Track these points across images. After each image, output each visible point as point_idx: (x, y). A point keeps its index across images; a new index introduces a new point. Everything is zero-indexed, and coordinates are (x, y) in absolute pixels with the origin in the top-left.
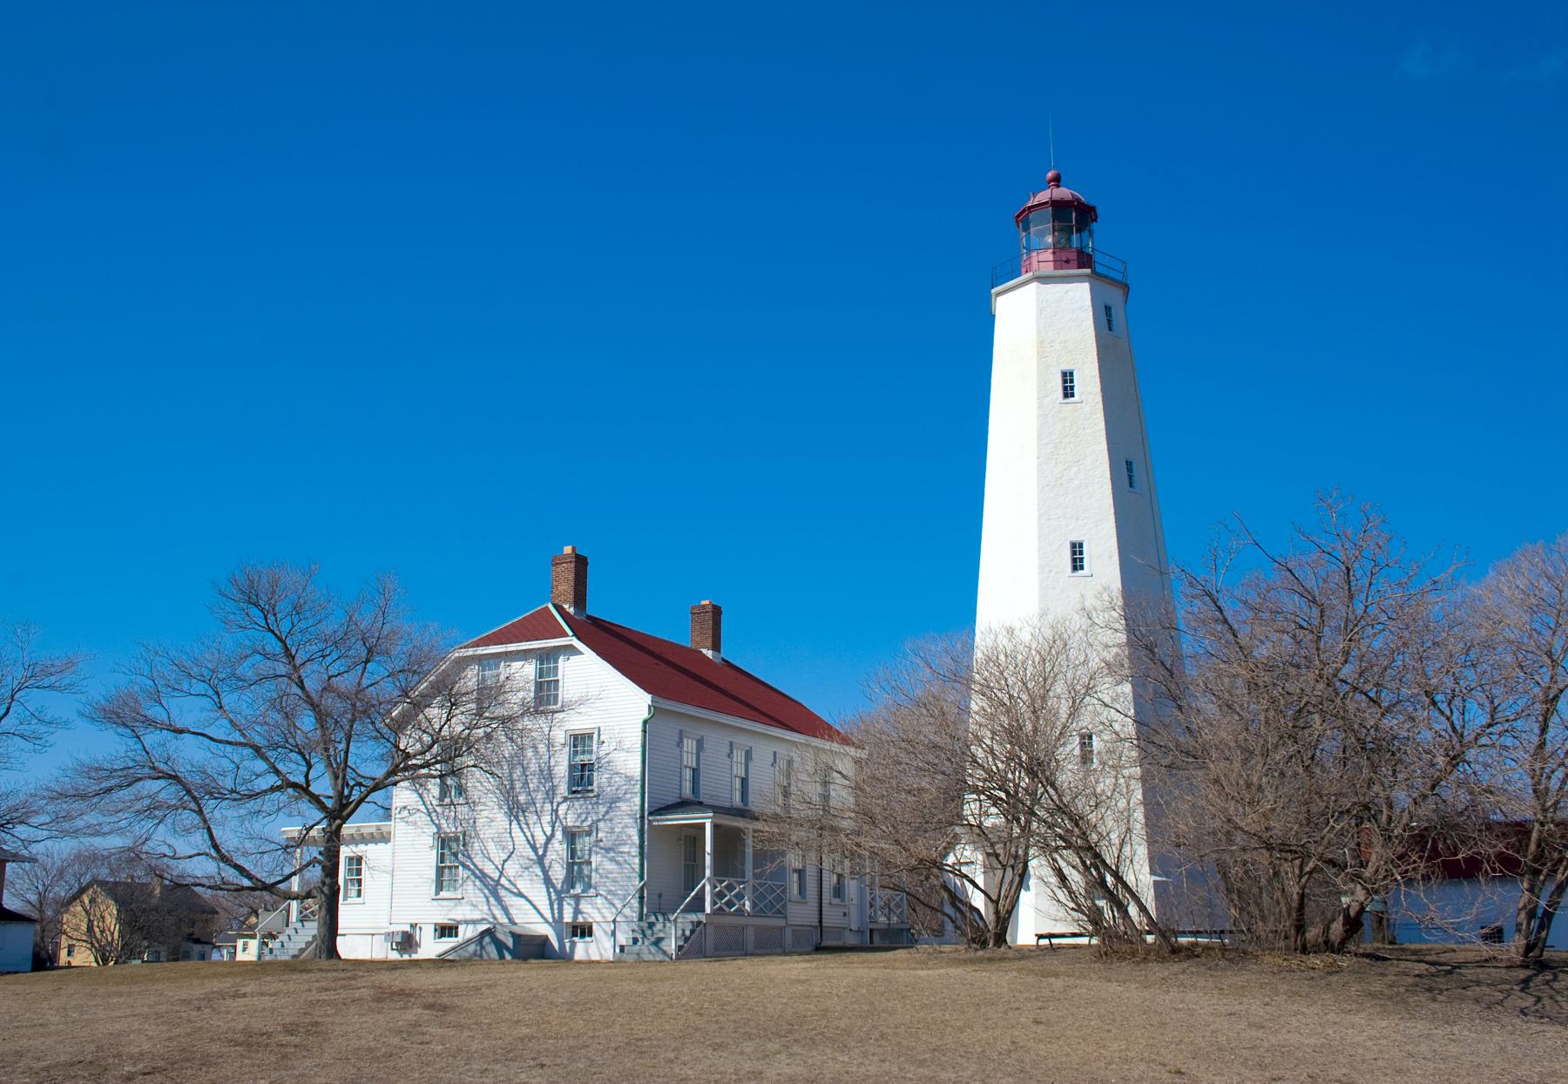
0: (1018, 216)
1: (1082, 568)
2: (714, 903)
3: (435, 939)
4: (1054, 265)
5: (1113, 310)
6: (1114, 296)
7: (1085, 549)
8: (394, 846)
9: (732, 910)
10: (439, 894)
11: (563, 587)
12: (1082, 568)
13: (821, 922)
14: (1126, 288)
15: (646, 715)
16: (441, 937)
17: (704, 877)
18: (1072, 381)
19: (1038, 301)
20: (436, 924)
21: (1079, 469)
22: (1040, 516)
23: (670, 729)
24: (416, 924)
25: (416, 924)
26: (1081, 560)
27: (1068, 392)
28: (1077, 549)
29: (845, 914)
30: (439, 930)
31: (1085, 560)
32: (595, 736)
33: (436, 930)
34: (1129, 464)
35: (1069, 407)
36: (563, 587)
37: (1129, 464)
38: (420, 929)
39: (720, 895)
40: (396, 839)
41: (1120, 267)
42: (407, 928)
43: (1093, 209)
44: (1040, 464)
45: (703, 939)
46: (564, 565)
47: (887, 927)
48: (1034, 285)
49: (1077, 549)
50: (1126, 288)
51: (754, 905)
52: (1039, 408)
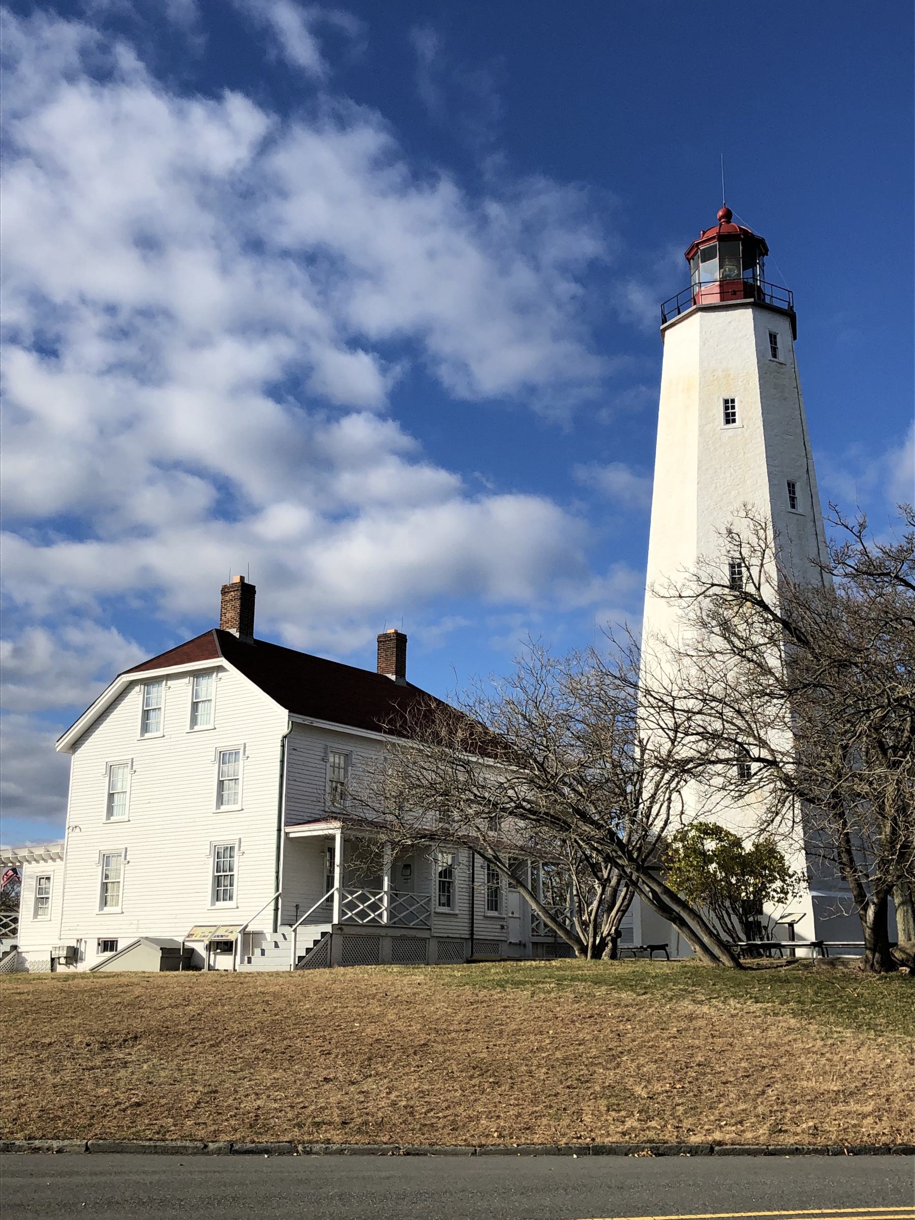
0: (688, 254)
1: (734, 421)
2: (342, 913)
3: (98, 953)
4: (721, 296)
5: (778, 337)
6: (782, 326)
7: (736, 404)
8: (66, 864)
9: (365, 921)
10: (102, 910)
11: (230, 614)
12: (734, 421)
13: (472, 934)
14: (790, 315)
15: (285, 730)
16: (104, 951)
17: (333, 887)
18: (733, 407)
19: (701, 332)
20: (99, 939)
21: (739, 492)
22: (698, 539)
23: (313, 746)
24: (81, 940)
25: (81, 940)
26: (734, 414)
27: (730, 418)
28: (729, 404)
29: (502, 927)
30: (102, 945)
31: (737, 414)
32: (241, 751)
33: (99, 944)
34: (791, 486)
35: (730, 433)
36: (230, 614)
37: (791, 486)
38: (86, 942)
39: (351, 906)
40: (68, 857)
41: (785, 295)
42: (73, 944)
43: (762, 242)
44: (699, 489)
45: (329, 951)
46: (232, 593)
47: (890, 940)
48: (699, 314)
49: (729, 404)
50: (790, 315)
51: (391, 916)
52: (700, 435)
